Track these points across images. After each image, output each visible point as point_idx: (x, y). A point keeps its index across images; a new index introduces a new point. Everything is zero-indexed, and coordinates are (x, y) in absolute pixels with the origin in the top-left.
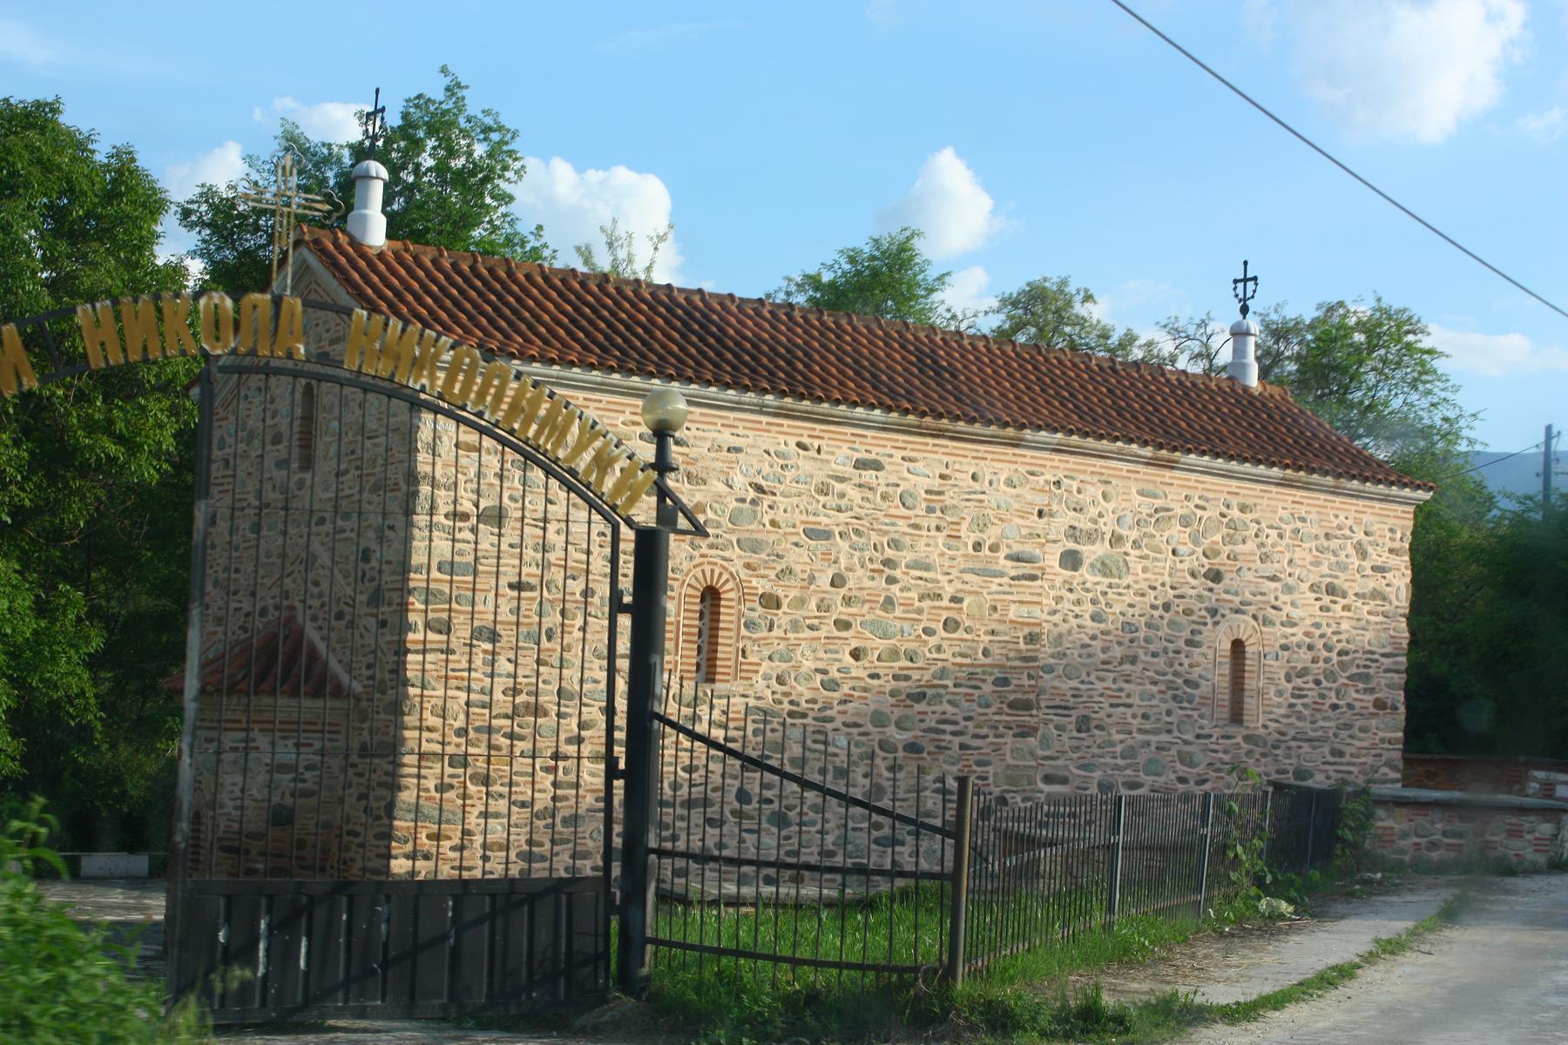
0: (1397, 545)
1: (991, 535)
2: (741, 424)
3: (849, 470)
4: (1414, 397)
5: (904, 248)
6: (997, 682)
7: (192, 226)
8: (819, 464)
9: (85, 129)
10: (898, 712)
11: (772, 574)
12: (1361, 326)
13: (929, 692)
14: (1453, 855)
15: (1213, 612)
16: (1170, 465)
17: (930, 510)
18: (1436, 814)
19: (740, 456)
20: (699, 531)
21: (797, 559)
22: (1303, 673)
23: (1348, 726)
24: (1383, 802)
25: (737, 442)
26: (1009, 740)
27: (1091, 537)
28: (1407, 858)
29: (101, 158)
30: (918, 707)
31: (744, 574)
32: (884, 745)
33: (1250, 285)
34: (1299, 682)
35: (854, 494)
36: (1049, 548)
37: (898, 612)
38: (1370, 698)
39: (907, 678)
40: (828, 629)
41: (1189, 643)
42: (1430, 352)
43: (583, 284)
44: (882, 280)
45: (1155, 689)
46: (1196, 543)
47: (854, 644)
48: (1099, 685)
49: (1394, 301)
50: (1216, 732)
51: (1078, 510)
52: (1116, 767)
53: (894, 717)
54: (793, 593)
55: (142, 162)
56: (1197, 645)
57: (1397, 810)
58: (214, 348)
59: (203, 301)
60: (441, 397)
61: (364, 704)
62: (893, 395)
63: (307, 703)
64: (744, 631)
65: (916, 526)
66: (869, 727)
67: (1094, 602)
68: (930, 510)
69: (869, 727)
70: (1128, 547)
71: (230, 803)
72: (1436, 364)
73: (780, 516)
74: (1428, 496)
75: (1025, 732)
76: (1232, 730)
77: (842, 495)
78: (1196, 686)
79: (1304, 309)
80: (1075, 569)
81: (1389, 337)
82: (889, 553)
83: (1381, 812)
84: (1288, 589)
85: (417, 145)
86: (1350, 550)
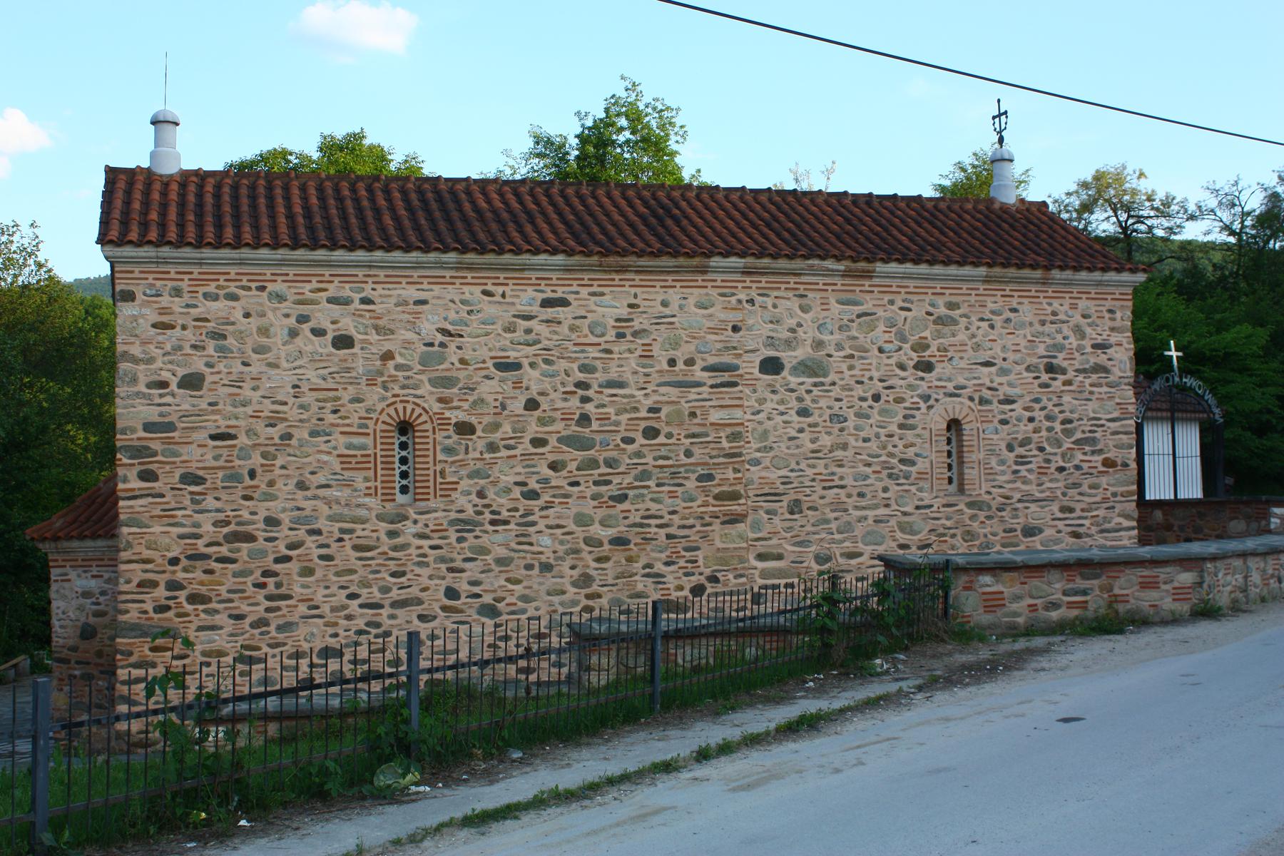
8: (505, 307)
19: (425, 307)
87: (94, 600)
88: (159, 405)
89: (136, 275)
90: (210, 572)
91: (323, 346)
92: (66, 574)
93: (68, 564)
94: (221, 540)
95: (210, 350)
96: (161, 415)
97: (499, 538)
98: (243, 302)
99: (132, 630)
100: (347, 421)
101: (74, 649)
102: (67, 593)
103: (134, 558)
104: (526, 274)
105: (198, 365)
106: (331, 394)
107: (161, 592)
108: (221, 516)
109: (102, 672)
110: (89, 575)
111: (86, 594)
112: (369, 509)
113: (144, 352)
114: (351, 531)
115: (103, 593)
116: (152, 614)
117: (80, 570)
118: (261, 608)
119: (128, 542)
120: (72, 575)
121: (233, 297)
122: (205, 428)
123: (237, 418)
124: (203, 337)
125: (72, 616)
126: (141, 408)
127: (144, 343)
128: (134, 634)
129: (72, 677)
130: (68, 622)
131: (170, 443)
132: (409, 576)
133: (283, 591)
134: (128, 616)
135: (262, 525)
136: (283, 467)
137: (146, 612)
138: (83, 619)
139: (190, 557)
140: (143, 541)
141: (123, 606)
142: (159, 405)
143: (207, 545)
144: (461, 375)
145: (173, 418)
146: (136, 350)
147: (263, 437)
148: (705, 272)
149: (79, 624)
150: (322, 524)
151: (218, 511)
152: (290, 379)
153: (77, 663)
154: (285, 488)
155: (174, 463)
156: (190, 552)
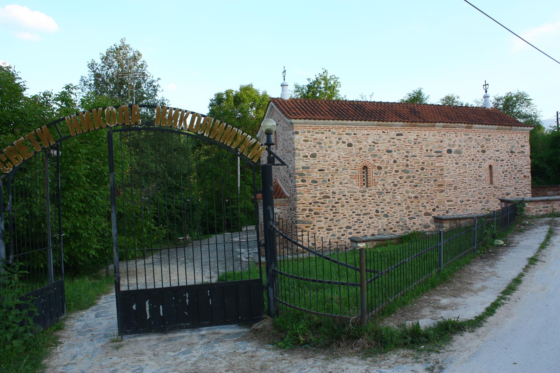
0: (526, 140)
1: (429, 148)
3: (395, 136)
4: (527, 109)
5: (419, 93)
6: (434, 181)
10: (412, 190)
11: (379, 162)
12: (515, 96)
14: (545, 212)
15: (484, 160)
16: (471, 128)
17: (415, 143)
18: (541, 203)
20: (283, 164)
21: (385, 157)
22: (506, 171)
23: (518, 182)
24: (527, 202)
25: (368, 133)
26: (438, 193)
27: (453, 146)
28: (534, 214)
30: (416, 188)
31: (373, 162)
32: (409, 197)
34: (505, 173)
35: (396, 141)
36: (444, 149)
37: (410, 167)
38: (522, 175)
39: (413, 182)
40: (394, 173)
41: (479, 167)
42: (530, 99)
43: (333, 102)
44: (417, 98)
46: (479, 145)
47: (400, 175)
48: (458, 179)
49: (521, 91)
50: (487, 187)
51: (450, 140)
52: (464, 197)
54: (384, 165)
56: (481, 167)
57: (531, 203)
58: (111, 125)
59: (106, 110)
60: (188, 130)
62: (404, 119)
64: (374, 175)
65: (412, 147)
66: (405, 194)
67: (456, 160)
68: (415, 143)
69: (405, 194)
70: (462, 147)
72: (531, 101)
73: (380, 148)
74: (532, 128)
75: (442, 191)
76: (490, 186)
77: (394, 142)
78: (481, 177)
79: (503, 94)
80: (451, 153)
81: (521, 98)
82: (406, 154)
83: (527, 204)
84: (501, 153)
85: (320, 83)
86: (515, 142)
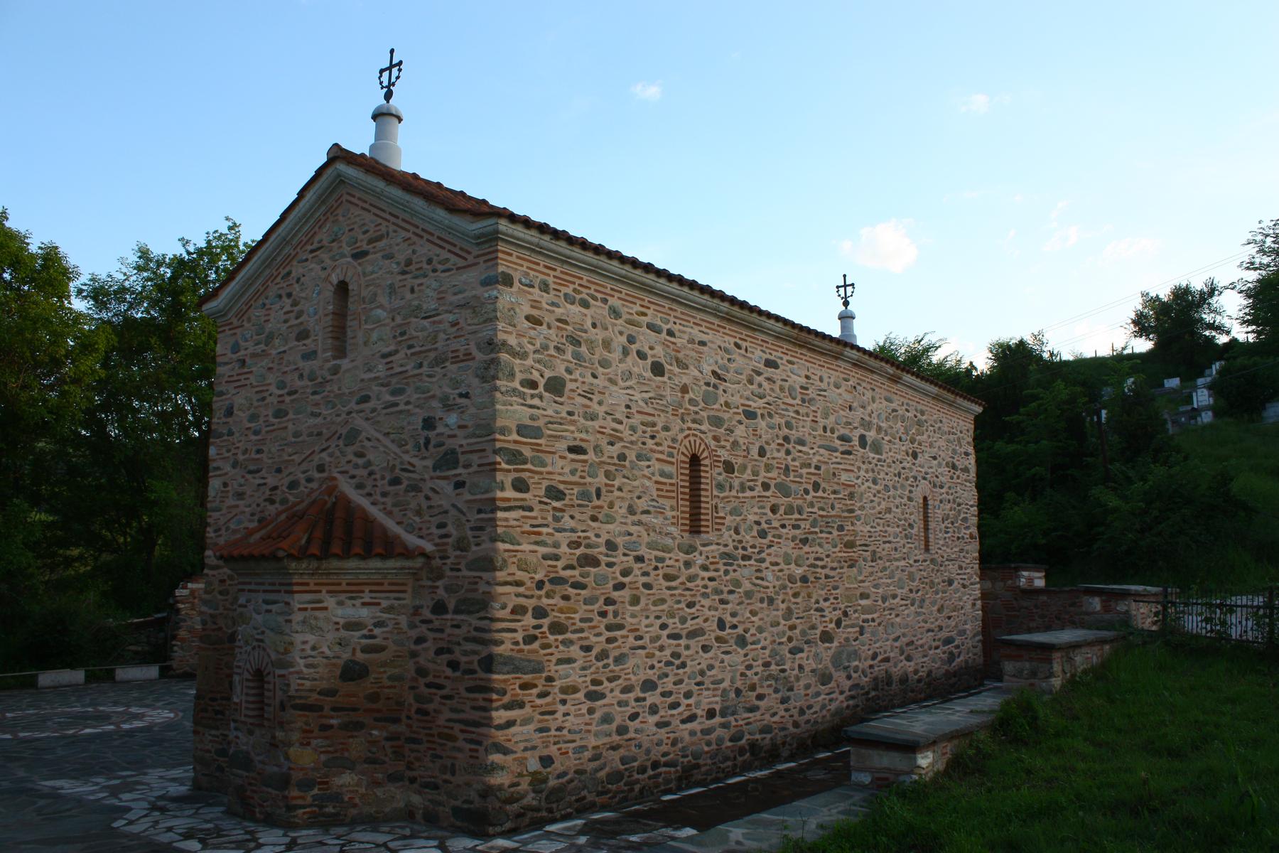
2: (704, 324)
7: (85, 297)
8: (747, 361)
9: (23, 231)
13: (810, 537)
19: (705, 349)
25: (704, 338)
29: (33, 249)
30: (806, 549)
33: (849, 289)
45: (898, 530)
53: (794, 556)
55: (63, 250)
61: (437, 562)
63: (376, 564)
71: (302, 662)
87: (365, 632)
88: (531, 407)
89: (514, 259)
90: (566, 598)
91: (643, 368)
92: (320, 601)
93: (324, 589)
94: (575, 564)
95: (569, 356)
96: (532, 418)
97: (746, 572)
98: (592, 310)
99: (505, 664)
100: (660, 448)
101: (331, 693)
102: (321, 624)
103: (509, 579)
104: (757, 335)
105: (560, 370)
106: (650, 419)
107: (529, 620)
108: (574, 537)
109: (376, 720)
110: (358, 602)
111: (352, 626)
112: (674, 538)
113: (520, 344)
114: (662, 560)
115: (379, 624)
116: (522, 646)
117: (343, 597)
118: (602, 639)
119: (505, 561)
120: (330, 602)
121: (585, 304)
122: (565, 438)
123: (587, 432)
124: (564, 341)
125: (328, 652)
126: (516, 407)
127: (519, 335)
128: (506, 669)
129: (325, 728)
130: (319, 660)
131: (538, 451)
132: (697, 607)
133: (618, 620)
134: (502, 647)
135: (603, 549)
136: (620, 489)
137: (517, 643)
138: (346, 656)
139: (552, 581)
140: (515, 560)
141: (498, 636)
142: (531, 407)
143: (565, 568)
144: (726, 416)
145: (540, 423)
146: (512, 341)
147: (606, 454)
148: (837, 358)
149: (341, 662)
150: (643, 551)
151: (573, 530)
152: (624, 400)
153: (334, 709)
154: (620, 510)
155: (541, 473)
156: (552, 575)
